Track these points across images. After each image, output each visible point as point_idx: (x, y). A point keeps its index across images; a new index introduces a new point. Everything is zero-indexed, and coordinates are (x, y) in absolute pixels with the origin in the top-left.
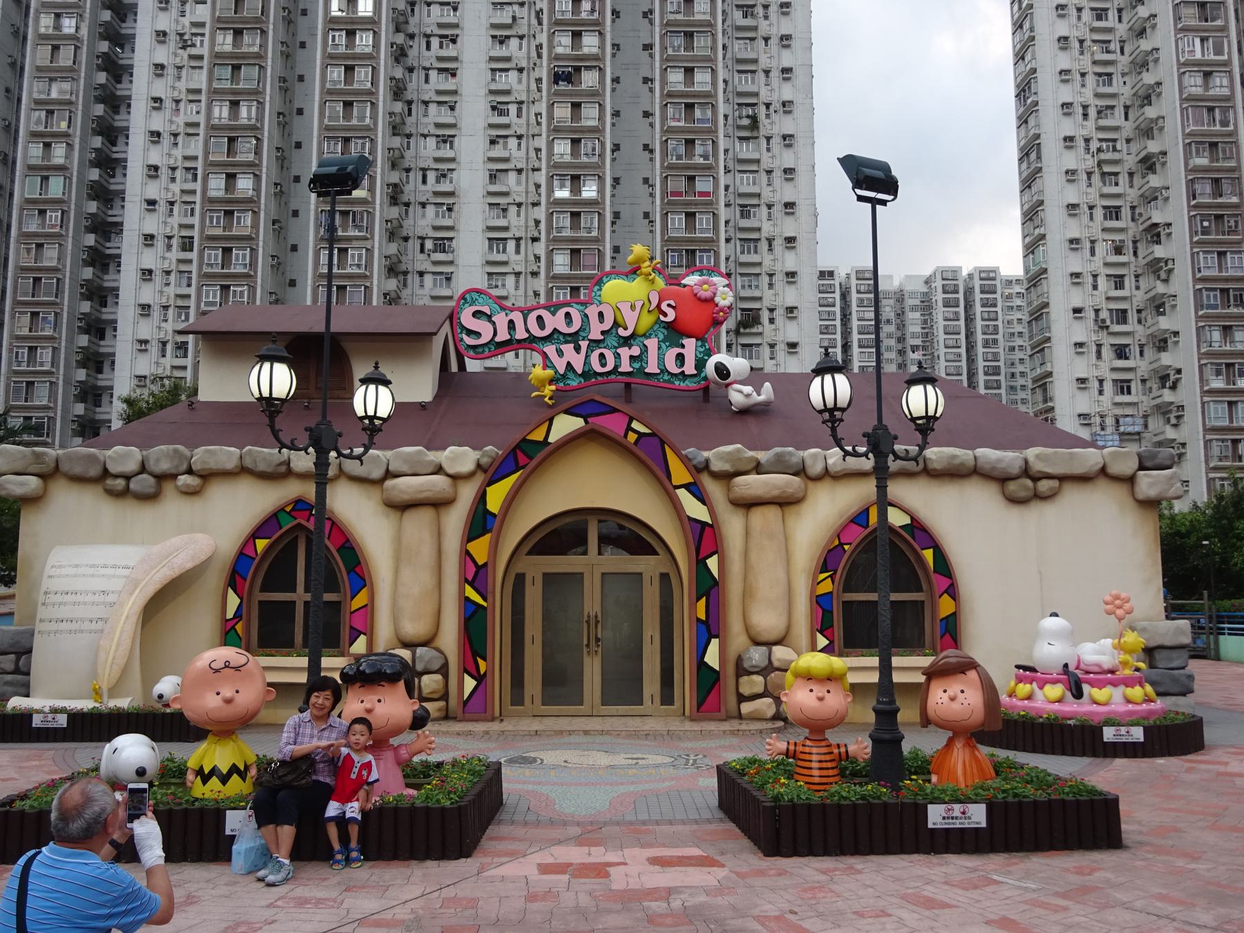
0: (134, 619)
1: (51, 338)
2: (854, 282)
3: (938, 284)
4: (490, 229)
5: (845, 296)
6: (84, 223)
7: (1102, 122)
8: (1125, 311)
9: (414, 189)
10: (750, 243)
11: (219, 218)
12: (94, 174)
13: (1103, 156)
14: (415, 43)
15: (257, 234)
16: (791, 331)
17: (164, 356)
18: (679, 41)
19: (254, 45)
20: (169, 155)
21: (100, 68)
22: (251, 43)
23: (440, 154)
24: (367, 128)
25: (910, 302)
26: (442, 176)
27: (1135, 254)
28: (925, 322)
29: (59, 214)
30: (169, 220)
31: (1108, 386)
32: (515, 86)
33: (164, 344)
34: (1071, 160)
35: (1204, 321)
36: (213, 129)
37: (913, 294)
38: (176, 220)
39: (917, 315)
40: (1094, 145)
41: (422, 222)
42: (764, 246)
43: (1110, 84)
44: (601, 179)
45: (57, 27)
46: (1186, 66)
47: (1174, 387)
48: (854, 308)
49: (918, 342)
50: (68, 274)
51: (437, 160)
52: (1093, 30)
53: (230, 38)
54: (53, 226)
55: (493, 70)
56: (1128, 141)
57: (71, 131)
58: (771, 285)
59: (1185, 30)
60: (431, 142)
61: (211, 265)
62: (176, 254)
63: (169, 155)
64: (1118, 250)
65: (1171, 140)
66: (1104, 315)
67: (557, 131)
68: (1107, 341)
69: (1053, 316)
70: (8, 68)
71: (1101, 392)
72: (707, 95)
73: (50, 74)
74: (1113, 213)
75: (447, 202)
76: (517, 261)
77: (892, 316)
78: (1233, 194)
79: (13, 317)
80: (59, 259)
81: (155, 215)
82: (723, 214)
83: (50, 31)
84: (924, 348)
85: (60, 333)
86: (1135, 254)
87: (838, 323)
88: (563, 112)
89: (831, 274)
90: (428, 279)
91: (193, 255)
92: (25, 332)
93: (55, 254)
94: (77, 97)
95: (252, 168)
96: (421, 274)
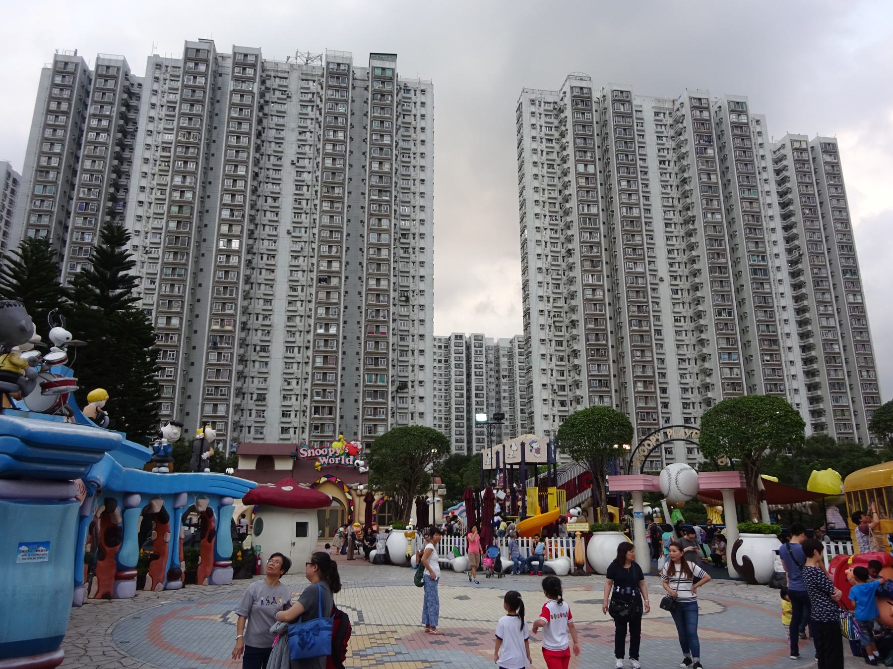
2: (473, 341)
4: (287, 342)
5: (468, 348)
7: (555, 305)
9: (253, 323)
10: (404, 352)
13: (555, 319)
14: (256, 257)
16: (421, 392)
18: (374, 266)
23: (265, 307)
24: (234, 299)
25: (502, 352)
26: (265, 317)
28: (510, 363)
32: (301, 278)
39: (506, 359)
40: (552, 314)
41: (255, 338)
42: (410, 353)
44: (338, 325)
45: (83, 239)
46: (586, 286)
48: (473, 355)
49: (506, 373)
51: (263, 310)
53: (172, 256)
55: (291, 271)
58: (413, 371)
59: (586, 271)
60: (261, 302)
67: (319, 303)
68: (557, 398)
69: (534, 387)
72: (386, 290)
74: (560, 343)
75: (267, 330)
76: (298, 357)
82: (391, 340)
84: (509, 377)
87: (464, 363)
88: (322, 295)
89: (461, 337)
90: (257, 364)
95: (179, 314)
96: (254, 361)
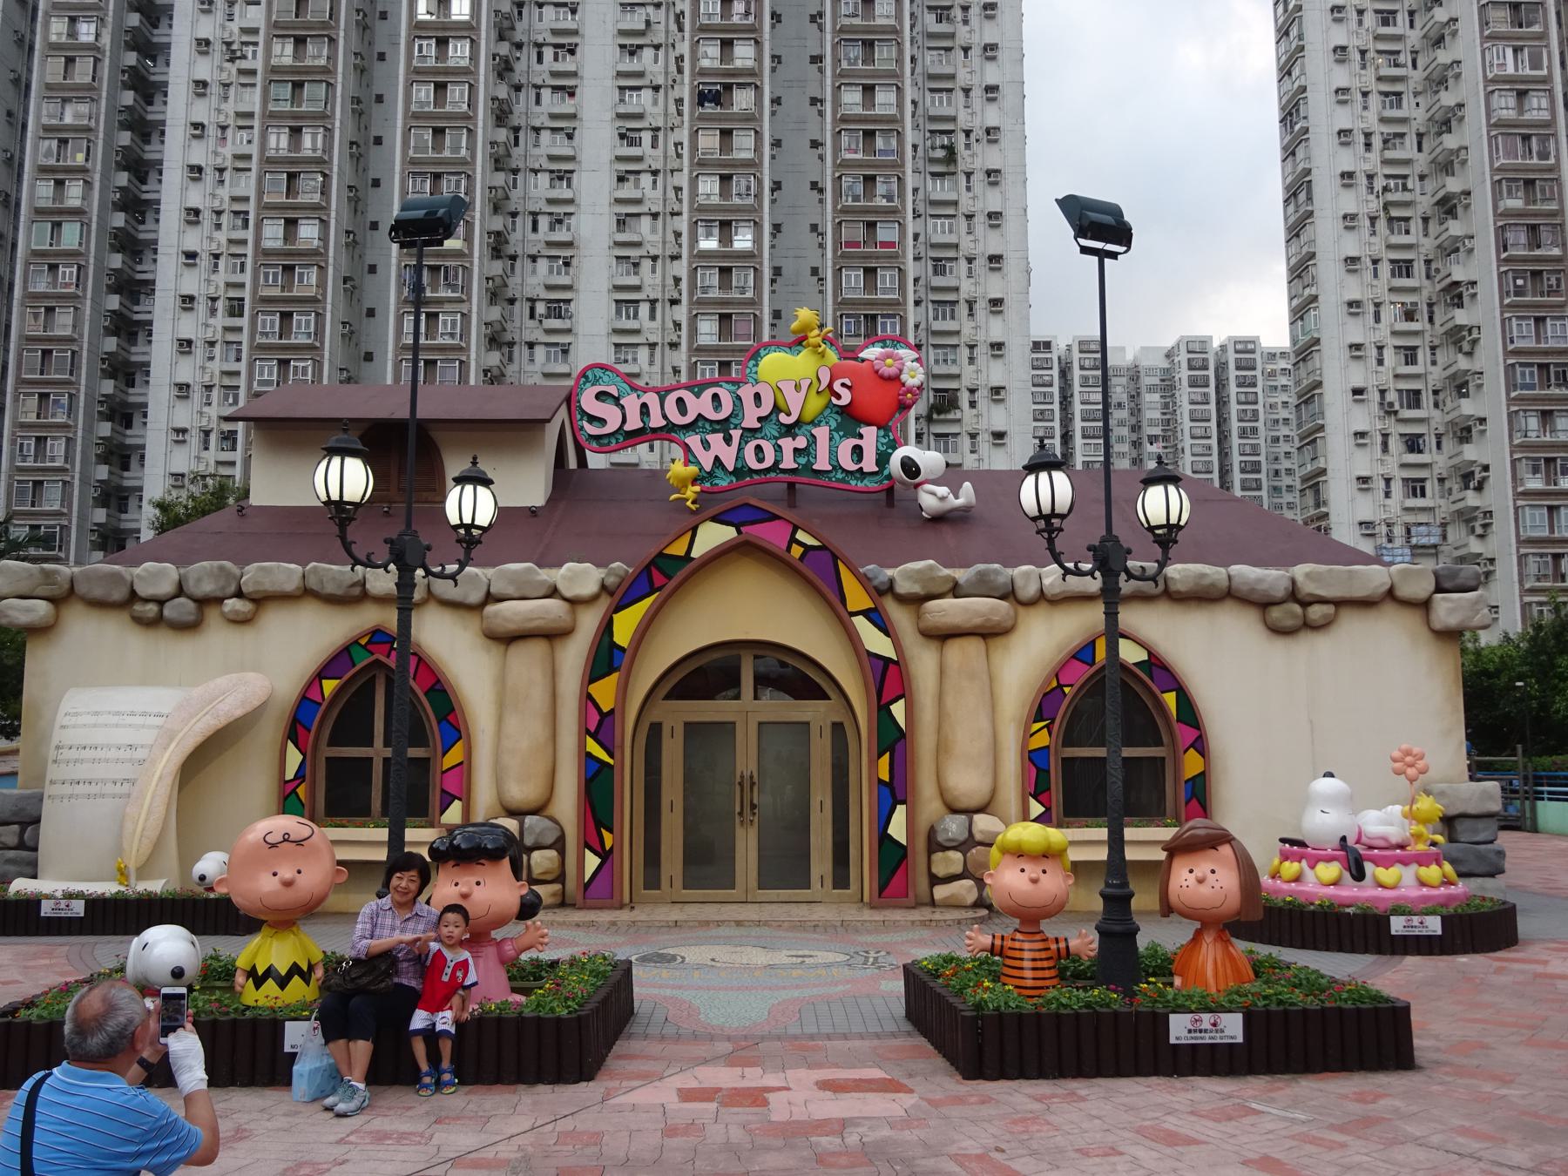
0: (169, 780)
1: (65, 426)
2: (1076, 355)
3: (1183, 357)
4: (618, 288)
5: (1065, 373)
6: (106, 281)
7: (1390, 154)
8: (1417, 392)
9: (522, 239)
10: (946, 307)
11: (275, 275)
12: (119, 220)
13: (1390, 197)
14: (523, 54)
15: (324, 295)
16: (996, 418)
17: (206, 449)
18: (856, 51)
19: (320, 57)
20: (214, 196)
21: (126, 86)
22: (316, 55)
23: (555, 194)
24: (463, 162)
25: (1147, 381)
26: (557, 222)
27: (1431, 320)
28: (1166, 406)
29: (75, 270)
30: (213, 277)
31: (1397, 487)
32: (650, 109)
33: (207, 433)
34: (1350, 202)
35: (1518, 405)
36: (269, 162)
37: (1150, 371)
38: (222, 277)
39: (1156, 397)
40: (1379, 183)
41: (532, 280)
42: (962, 310)
43: (1399, 106)
44: (757, 225)
45: (72, 34)
46: (1495, 83)
47: (1479, 488)
48: (1077, 388)
49: (1157, 431)
50: (85, 346)
51: (550, 201)
52: (1377, 38)
53: (289, 48)
54: (67, 285)
55: (622, 88)
56: (1422, 178)
57: (89, 165)
58: (972, 360)
59: (1494, 37)
60: (544, 179)
61: (266, 334)
62: (221, 320)
63: (214, 196)
64: (1409, 316)
65: (1476, 176)
66: (1392, 396)
67: (702, 165)
68: (1396, 429)
69: (1327, 398)
70: (10, 86)
71: (1387, 495)
72: (891, 120)
73: (63, 94)
74: (1403, 268)
75: (564, 254)
76: (651, 329)
77: (1124, 398)
78: (1554, 244)
79: (16, 399)
80: (74, 327)
81: (195, 271)
82: (912, 269)
83: (64, 39)
84: (1165, 439)
85: (76, 420)
86: (1431, 320)
87: (1056, 407)
88: (709, 141)
89: (1047, 345)
90: (540, 352)
91: (244, 322)
92: (32, 418)
93: (69, 320)
94: (97, 122)
95: (318, 211)
96: (531, 345)
